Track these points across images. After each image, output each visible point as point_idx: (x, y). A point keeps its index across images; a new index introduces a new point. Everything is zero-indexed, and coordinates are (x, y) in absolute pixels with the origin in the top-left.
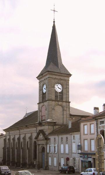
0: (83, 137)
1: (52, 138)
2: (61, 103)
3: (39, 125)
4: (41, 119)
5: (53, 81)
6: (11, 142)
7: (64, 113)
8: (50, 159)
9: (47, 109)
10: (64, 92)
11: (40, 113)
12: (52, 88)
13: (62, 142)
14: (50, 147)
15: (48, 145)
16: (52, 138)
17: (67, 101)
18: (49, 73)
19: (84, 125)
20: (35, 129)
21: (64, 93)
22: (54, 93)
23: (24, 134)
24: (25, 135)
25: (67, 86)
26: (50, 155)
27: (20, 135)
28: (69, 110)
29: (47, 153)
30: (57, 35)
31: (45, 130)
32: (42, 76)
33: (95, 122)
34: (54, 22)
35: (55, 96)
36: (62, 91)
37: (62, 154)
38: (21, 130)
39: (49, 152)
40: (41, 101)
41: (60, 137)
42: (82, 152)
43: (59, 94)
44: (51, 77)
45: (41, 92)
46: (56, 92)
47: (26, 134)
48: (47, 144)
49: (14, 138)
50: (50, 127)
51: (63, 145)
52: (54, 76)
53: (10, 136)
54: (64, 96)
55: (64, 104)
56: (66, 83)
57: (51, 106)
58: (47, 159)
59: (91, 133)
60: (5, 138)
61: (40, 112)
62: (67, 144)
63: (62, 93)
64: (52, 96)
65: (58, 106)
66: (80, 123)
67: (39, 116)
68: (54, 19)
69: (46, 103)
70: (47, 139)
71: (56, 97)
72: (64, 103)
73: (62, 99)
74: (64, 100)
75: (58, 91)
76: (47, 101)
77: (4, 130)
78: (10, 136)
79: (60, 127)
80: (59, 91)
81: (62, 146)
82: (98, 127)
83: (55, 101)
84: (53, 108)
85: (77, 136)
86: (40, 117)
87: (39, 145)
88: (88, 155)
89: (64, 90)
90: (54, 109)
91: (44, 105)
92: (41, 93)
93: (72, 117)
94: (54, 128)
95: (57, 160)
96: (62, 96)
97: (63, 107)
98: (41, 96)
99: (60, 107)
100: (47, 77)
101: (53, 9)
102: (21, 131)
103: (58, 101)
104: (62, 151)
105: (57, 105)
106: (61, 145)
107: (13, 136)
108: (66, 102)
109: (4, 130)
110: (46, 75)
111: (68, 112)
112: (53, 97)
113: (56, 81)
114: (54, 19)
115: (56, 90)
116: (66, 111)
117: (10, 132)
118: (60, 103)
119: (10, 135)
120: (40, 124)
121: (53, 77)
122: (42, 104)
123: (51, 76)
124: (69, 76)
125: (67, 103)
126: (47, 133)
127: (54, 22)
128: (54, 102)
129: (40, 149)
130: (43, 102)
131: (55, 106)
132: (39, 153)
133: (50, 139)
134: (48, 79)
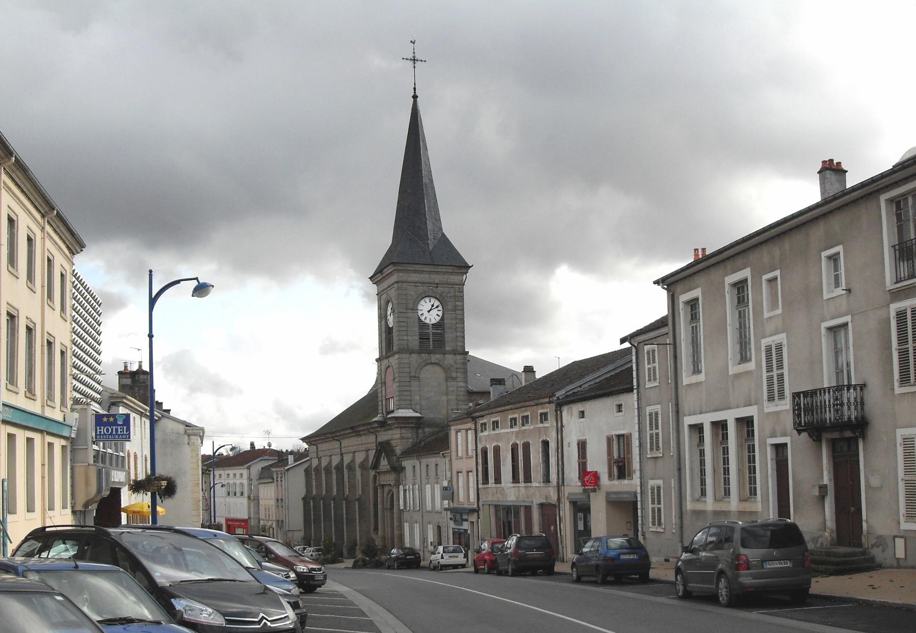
0: (457, 465)
1: (408, 464)
2: (438, 356)
3: (381, 427)
4: (386, 410)
5: (412, 291)
6: (357, 480)
7: (451, 389)
8: (406, 526)
9: (397, 380)
10: (446, 321)
11: (384, 388)
12: (410, 315)
13: (438, 477)
14: (405, 491)
15: (401, 487)
16: (408, 464)
17: (459, 348)
18: (399, 268)
19: (457, 432)
20: (372, 438)
21: (446, 326)
22: (417, 329)
23: (351, 454)
24: (354, 457)
25: (457, 303)
26: (406, 516)
27: (342, 454)
28: (466, 377)
29: (401, 512)
30: (424, 141)
31: (393, 443)
32: (382, 274)
33: (470, 425)
34: (415, 97)
35: (417, 338)
36: (442, 319)
37: (429, 512)
38: (342, 441)
39: (405, 508)
40: (384, 353)
41: (425, 461)
42: (455, 505)
43: (431, 331)
44: (404, 279)
45: (383, 322)
46: (423, 325)
47: (356, 454)
48: (398, 483)
49: (353, 461)
50: (408, 433)
51: (430, 486)
52: (412, 275)
53: (319, 459)
54: (449, 336)
55: (450, 359)
56: (452, 294)
57: (408, 370)
58: (401, 528)
59: (458, 456)
60: (306, 466)
61: (382, 387)
62: (437, 483)
63: (439, 325)
64: (410, 338)
65: (429, 367)
66: (450, 426)
67: (380, 399)
68: (415, 89)
69: (394, 361)
70: (398, 470)
71: (423, 338)
72: (448, 356)
73: (440, 342)
74: (448, 348)
75: (427, 321)
76: (395, 353)
77: (304, 439)
78: (319, 459)
79: (439, 432)
80: (434, 322)
81: (428, 487)
82: (478, 438)
83: (419, 353)
84: (413, 374)
85: (443, 462)
86: (384, 402)
87: (383, 486)
88: (461, 515)
89: (446, 316)
90: (417, 378)
91: (389, 366)
92: (383, 328)
93: (474, 397)
94: (417, 434)
95: (419, 529)
96: (442, 335)
97: (446, 370)
98: (384, 336)
99: (438, 369)
100: (394, 278)
101: (411, 56)
102: (345, 442)
103: (429, 353)
104: (429, 507)
105: (421, 369)
106: (427, 485)
107: (328, 459)
108: (455, 352)
109: (304, 439)
110: (391, 274)
111: (462, 384)
112: (414, 340)
113: (421, 289)
114: (415, 89)
115: (423, 318)
116: (455, 379)
117: (320, 446)
118: (435, 358)
119: (320, 454)
120: (383, 424)
121: (410, 279)
122: (385, 362)
123: (403, 276)
124: (463, 271)
125: (458, 357)
126: (398, 450)
127: (415, 97)
128: (414, 357)
129: (385, 499)
130: (387, 357)
131: (421, 367)
132: (383, 511)
133: (405, 468)
134: (396, 285)
